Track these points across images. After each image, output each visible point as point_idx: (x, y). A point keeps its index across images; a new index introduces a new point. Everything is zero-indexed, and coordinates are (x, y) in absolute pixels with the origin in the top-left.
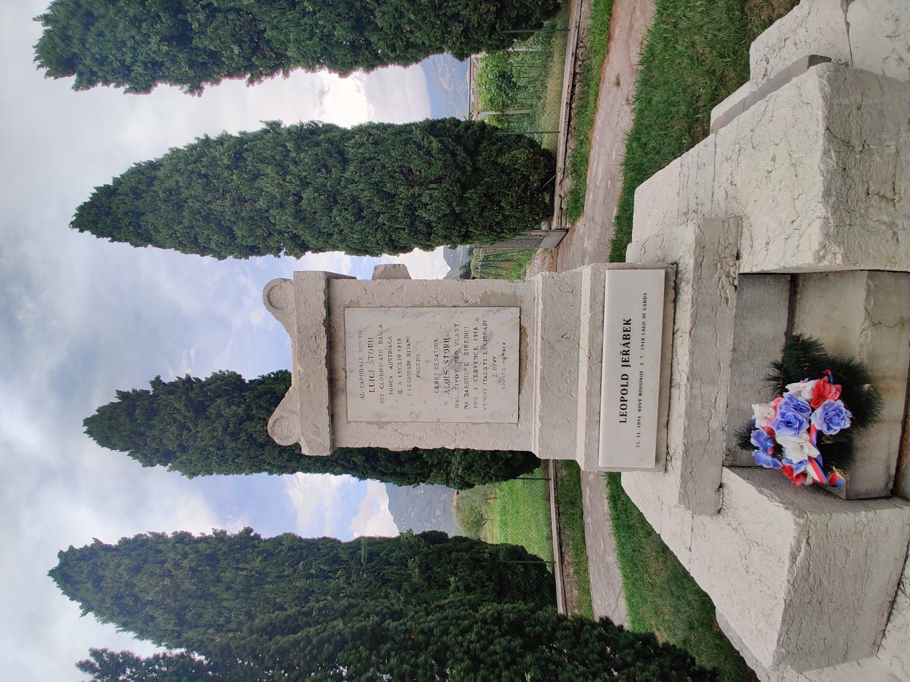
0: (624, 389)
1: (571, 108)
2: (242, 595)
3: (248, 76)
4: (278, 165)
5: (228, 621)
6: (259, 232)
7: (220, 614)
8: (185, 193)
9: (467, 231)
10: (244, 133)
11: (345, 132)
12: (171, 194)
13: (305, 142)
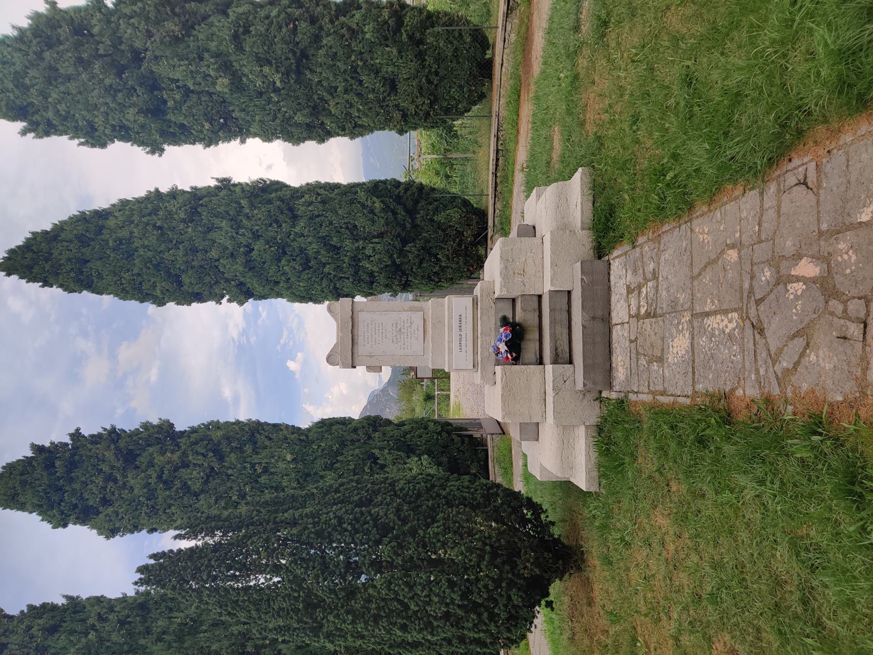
0: (460, 340)
1: (496, 177)
2: (174, 645)
4: (232, 220)
6: (207, 279)
8: (137, 243)
9: (407, 280)
11: (295, 190)
12: (121, 243)
13: (259, 199)
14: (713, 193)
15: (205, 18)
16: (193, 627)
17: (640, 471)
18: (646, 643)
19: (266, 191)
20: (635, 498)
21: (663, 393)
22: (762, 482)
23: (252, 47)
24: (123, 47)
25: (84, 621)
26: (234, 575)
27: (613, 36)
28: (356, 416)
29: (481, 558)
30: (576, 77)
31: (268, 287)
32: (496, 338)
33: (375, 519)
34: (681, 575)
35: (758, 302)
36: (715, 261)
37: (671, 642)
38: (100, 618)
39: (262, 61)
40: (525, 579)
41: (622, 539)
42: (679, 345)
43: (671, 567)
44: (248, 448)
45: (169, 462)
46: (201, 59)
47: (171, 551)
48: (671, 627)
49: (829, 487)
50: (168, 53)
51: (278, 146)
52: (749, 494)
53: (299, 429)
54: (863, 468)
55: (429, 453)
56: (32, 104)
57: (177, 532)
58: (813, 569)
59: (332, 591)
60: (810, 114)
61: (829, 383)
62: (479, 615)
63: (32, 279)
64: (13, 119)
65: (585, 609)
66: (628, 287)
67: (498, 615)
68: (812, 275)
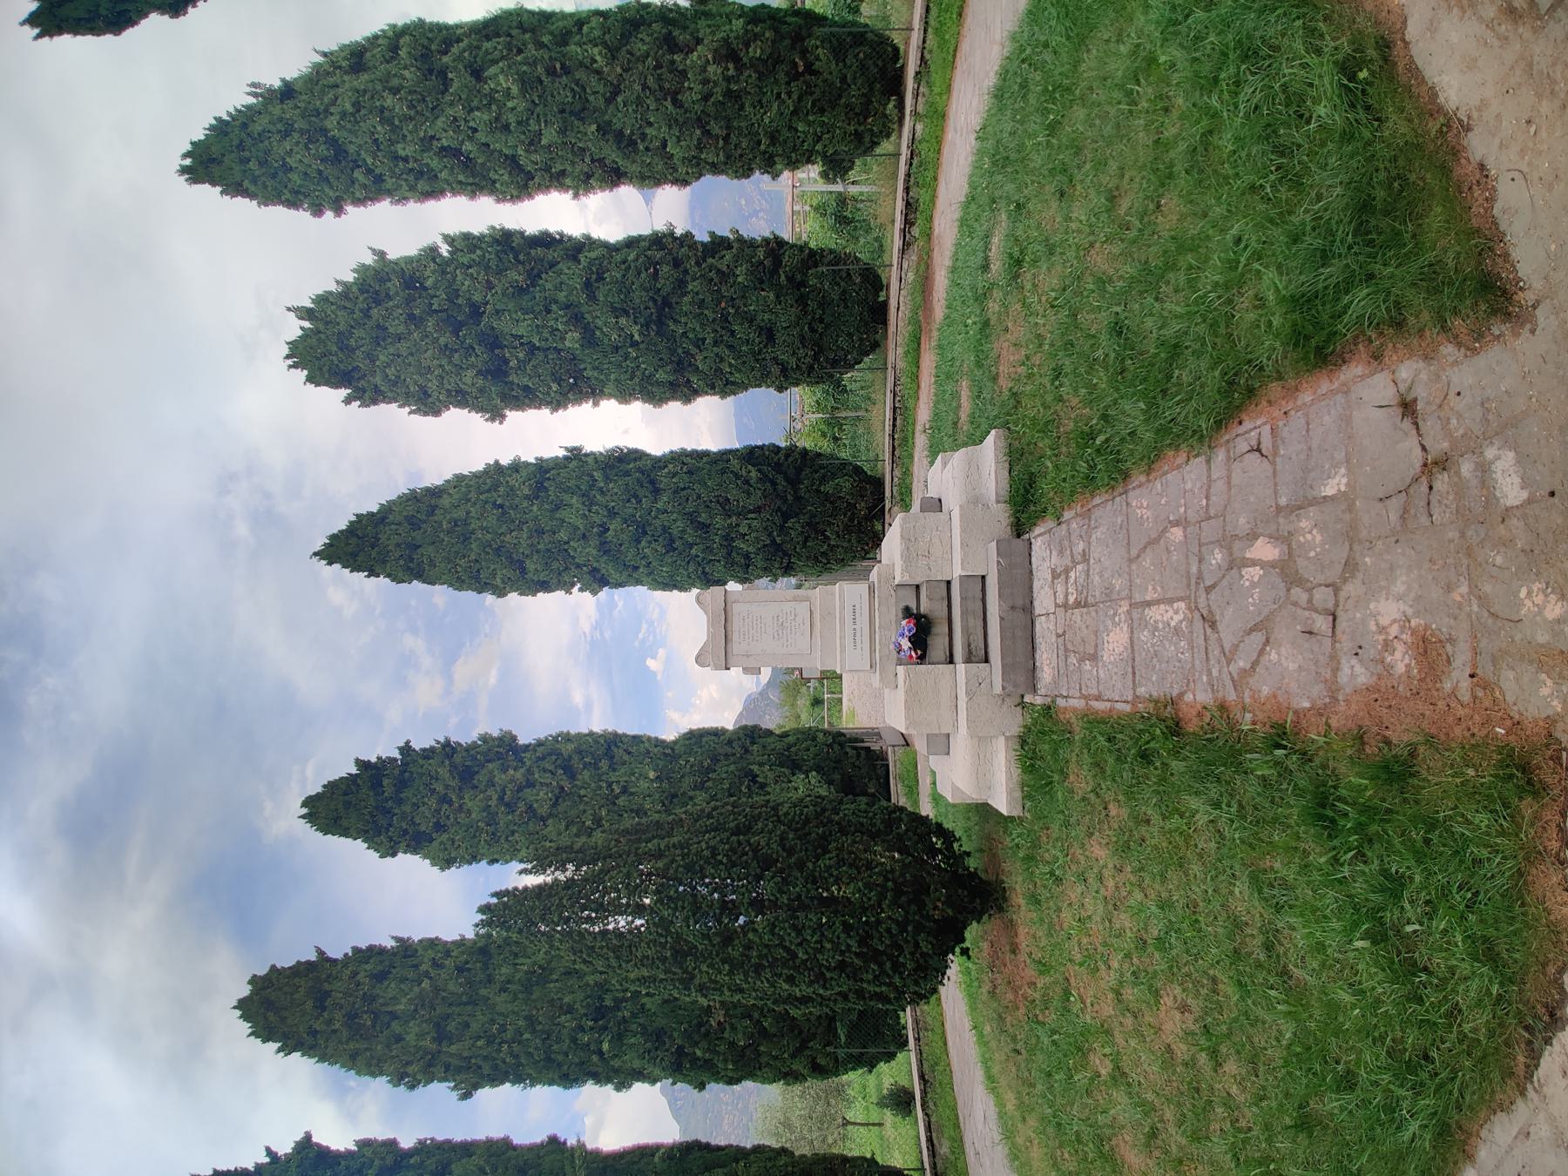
3: (37, 31)
5: (503, 1029)
6: (555, 565)
7: (493, 1021)
10: (541, 459)
14: (1152, 460)
15: (552, 265)
16: (540, 976)
17: (1072, 791)
18: (1081, 997)
19: (623, 462)
20: (1066, 824)
21: (1098, 698)
22: (1217, 805)
23: (606, 296)
24: (460, 301)
25: (416, 966)
26: (589, 917)
27: (1029, 276)
28: (730, 727)
29: (882, 897)
30: (986, 323)
31: (625, 574)
32: (899, 633)
33: (756, 850)
34: (1123, 916)
35: (1208, 590)
36: (1156, 541)
37: (1111, 996)
38: (436, 964)
39: (618, 312)
40: (935, 921)
41: (1052, 873)
42: (1115, 641)
43: (1110, 907)
44: (604, 764)
45: (511, 781)
46: (549, 311)
47: (516, 889)
48: (1111, 979)
49: (1295, 811)
50: (511, 306)
51: (637, 408)
52: (1201, 819)
53: (663, 741)
54: (1335, 787)
55: (819, 769)
56: (356, 368)
57: (523, 866)
58: (1278, 908)
59: (706, 936)
60: (1261, 369)
61: (1294, 685)
62: (881, 965)
63: (356, 568)
64: (336, 386)
65: (1008, 956)
66: (1053, 571)
67: (904, 965)
68: (1270, 558)
